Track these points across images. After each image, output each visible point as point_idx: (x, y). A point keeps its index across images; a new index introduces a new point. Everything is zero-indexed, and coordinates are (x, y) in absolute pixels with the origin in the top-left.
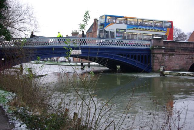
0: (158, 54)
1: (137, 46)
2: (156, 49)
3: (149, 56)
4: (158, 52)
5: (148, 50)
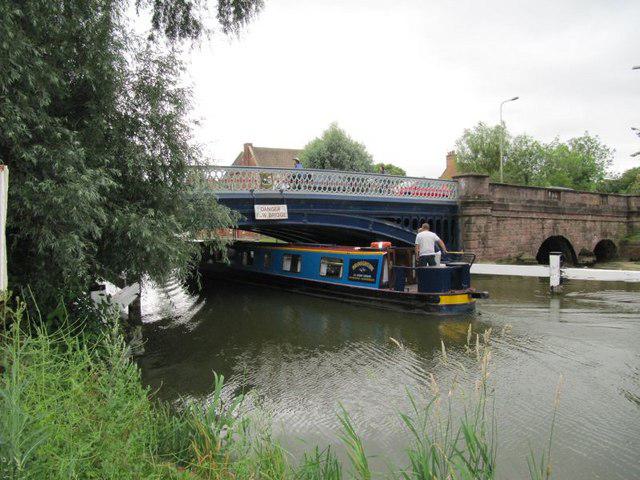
0: (478, 216)
1: (358, 190)
2: (474, 203)
3: (454, 223)
4: (478, 212)
5: (452, 208)
